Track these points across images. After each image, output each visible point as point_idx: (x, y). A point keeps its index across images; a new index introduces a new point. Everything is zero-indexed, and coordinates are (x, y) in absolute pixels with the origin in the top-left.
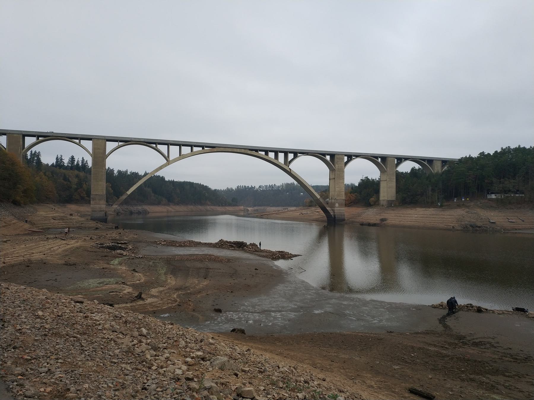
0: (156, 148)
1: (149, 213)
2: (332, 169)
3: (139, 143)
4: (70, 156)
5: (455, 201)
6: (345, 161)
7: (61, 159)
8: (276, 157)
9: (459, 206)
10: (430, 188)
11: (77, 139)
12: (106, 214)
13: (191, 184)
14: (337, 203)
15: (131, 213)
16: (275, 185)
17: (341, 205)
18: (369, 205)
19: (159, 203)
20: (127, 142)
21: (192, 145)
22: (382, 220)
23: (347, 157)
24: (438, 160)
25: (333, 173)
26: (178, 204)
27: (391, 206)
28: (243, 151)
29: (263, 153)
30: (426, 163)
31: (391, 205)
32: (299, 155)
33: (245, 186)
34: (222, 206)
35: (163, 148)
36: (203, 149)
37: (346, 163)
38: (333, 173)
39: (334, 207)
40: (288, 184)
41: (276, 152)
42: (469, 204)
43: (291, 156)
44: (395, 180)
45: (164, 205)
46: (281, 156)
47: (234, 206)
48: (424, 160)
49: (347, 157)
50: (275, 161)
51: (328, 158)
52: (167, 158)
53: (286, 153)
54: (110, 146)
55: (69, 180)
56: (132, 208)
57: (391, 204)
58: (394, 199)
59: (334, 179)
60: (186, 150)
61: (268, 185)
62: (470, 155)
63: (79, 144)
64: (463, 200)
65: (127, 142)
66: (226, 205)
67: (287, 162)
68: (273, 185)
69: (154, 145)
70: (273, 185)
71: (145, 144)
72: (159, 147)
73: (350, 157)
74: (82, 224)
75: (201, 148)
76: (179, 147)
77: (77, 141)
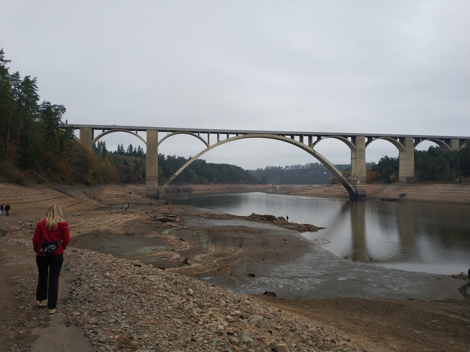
1: (193, 190)
3: (185, 132)
4: (129, 145)
7: (122, 147)
8: (301, 140)
12: (158, 192)
13: (227, 166)
14: (359, 180)
15: (179, 191)
16: (300, 165)
17: (362, 182)
19: (201, 183)
20: (175, 131)
22: (402, 195)
24: (455, 138)
26: (216, 183)
27: (410, 182)
28: (271, 136)
29: (290, 137)
30: (444, 142)
31: (410, 181)
32: (322, 137)
33: (273, 166)
34: (253, 184)
35: (204, 136)
36: (237, 135)
37: (367, 144)
40: (313, 164)
41: (301, 136)
43: (315, 139)
45: (206, 184)
46: (306, 139)
50: (300, 144)
51: (350, 139)
52: (207, 144)
53: (310, 136)
54: (161, 135)
55: (128, 164)
56: (179, 187)
58: (413, 175)
60: (223, 137)
63: (136, 135)
65: (175, 131)
66: (256, 183)
69: (197, 134)
71: (190, 133)
72: (201, 135)
73: (371, 138)
74: (139, 200)
75: (235, 135)
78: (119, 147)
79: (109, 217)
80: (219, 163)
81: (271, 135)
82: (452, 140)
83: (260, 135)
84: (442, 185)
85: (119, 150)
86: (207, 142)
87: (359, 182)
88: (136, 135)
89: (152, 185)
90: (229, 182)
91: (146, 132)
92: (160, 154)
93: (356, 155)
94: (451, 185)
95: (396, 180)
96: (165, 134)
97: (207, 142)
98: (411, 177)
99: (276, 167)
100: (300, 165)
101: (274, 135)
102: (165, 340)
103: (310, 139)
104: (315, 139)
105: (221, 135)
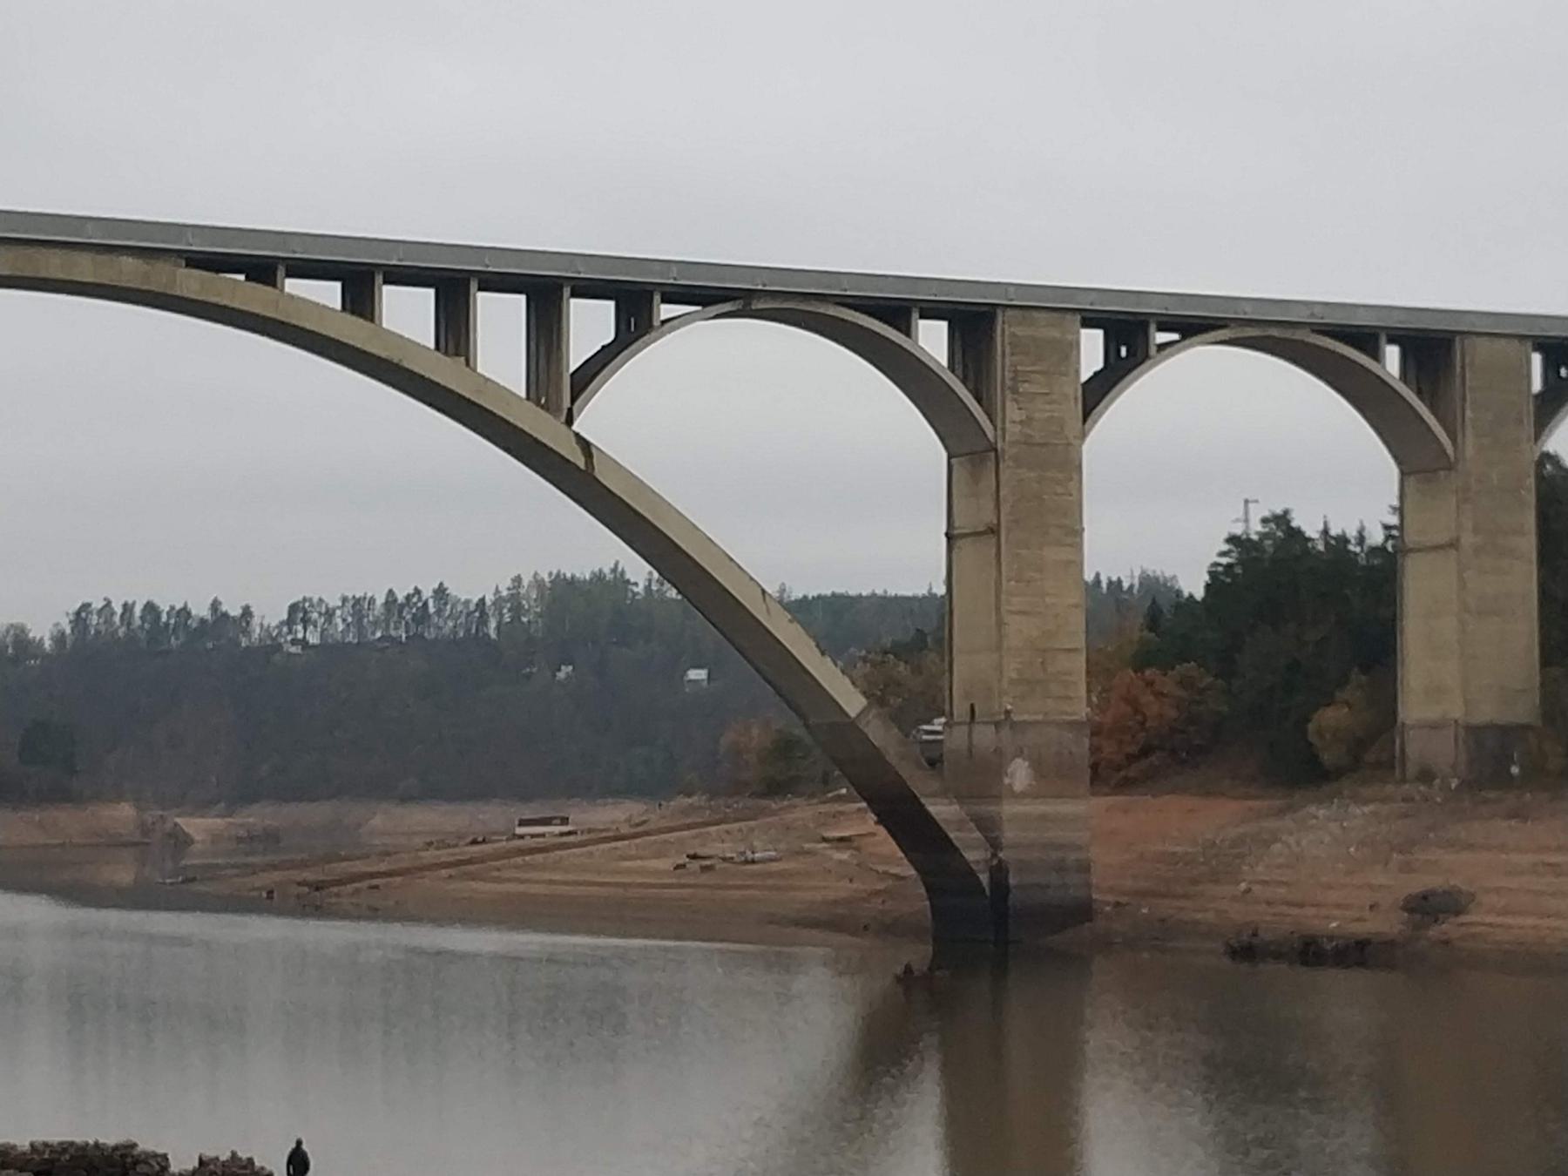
6: (1085, 375)
14: (1019, 753)
16: (440, 592)
29: (329, 293)
32: (666, 311)
33: (150, 608)
39: (997, 798)
40: (572, 583)
50: (444, 372)
51: (932, 339)
58: (1525, 710)
59: (993, 531)
61: (380, 600)
68: (427, 593)
70: (427, 593)
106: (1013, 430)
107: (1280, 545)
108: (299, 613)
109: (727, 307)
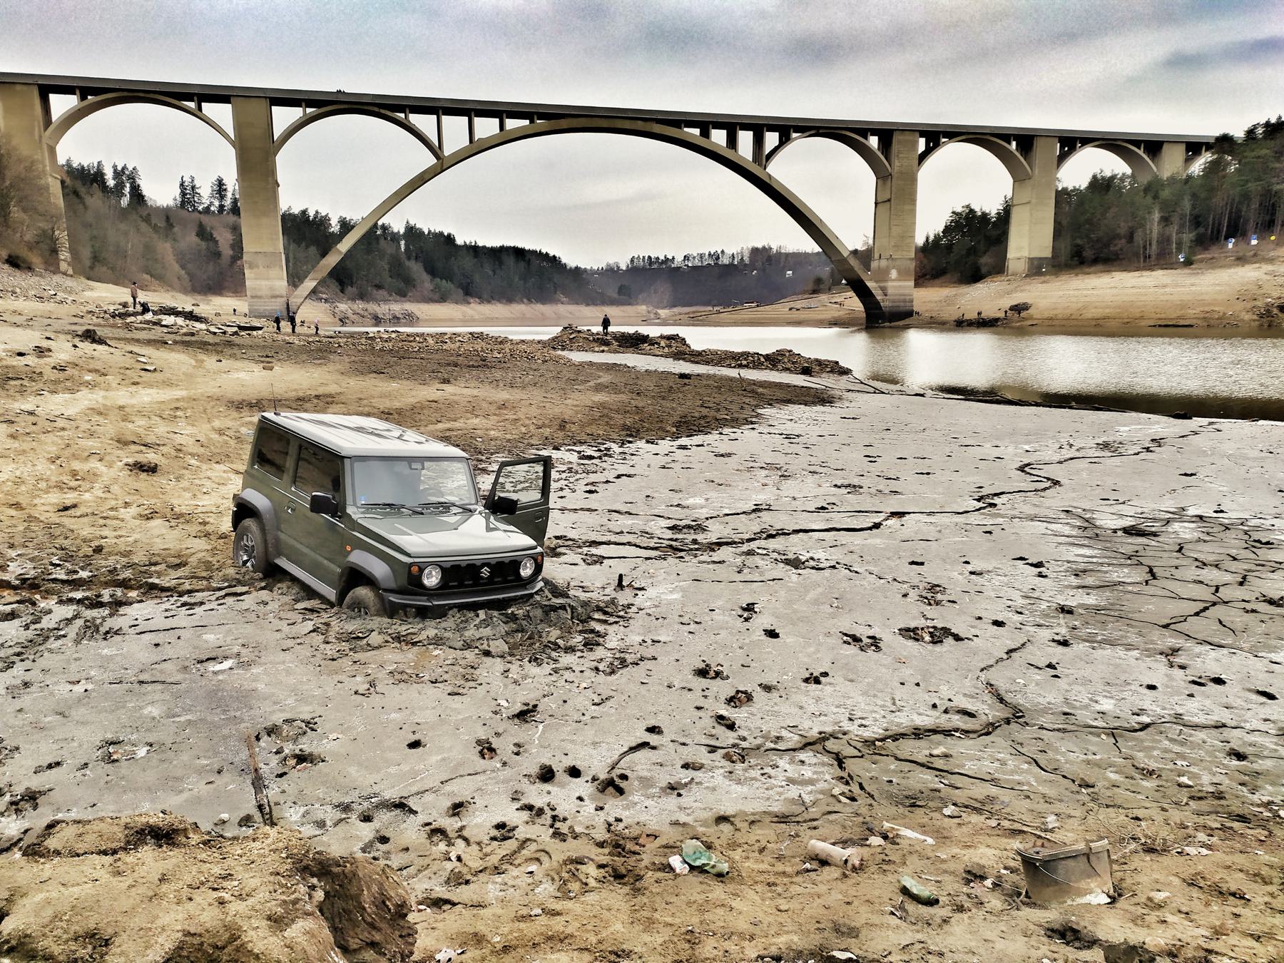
0: (405, 122)
2: (882, 176)
4: (214, 179)
5: (1230, 246)
6: (920, 152)
7: (193, 188)
8: (732, 142)
9: (1241, 260)
10: (1156, 216)
11: (189, 97)
14: (894, 267)
16: (723, 252)
17: (902, 274)
18: (975, 277)
19: (443, 299)
21: (499, 111)
22: (1019, 309)
23: (776, 135)
24: (1175, 140)
25: (884, 183)
27: (1041, 274)
28: (639, 125)
29: (696, 131)
30: (1141, 152)
31: (1037, 269)
32: (794, 135)
33: (650, 257)
35: (425, 123)
36: (532, 122)
37: (923, 157)
38: (884, 183)
39: (886, 281)
40: (757, 249)
42: (1272, 254)
43: (771, 139)
44: (1053, 201)
46: (745, 139)
47: (623, 304)
48: (1137, 141)
49: (776, 135)
50: (729, 154)
51: (873, 141)
52: (436, 151)
54: (283, 117)
55: (211, 235)
57: (1040, 267)
58: (1047, 253)
60: (487, 127)
62: (1280, 118)
63: (197, 114)
64: (1254, 242)
67: (761, 157)
71: (376, 109)
72: (416, 119)
73: (935, 136)
75: (527, 122)
76: (466, 119)
77: (192, 105)
78: (182, 185)
79: (1109, 692)
80: (494, 245)
81: (639, 122)
82: (1165, 146)
83: (605, 123)
84: (1137, 274)
85: (183, 194)
86: (437, 145)
87: (894, 274)
88: (198, 113)
89: (267, 283)
90: (525, 300)
91: (229, 106)
92: (317, 212)
93: (889, 192)
94: (1160, 272)
95: (999, 268)
96: (295, 113)
97: (434, 140)
98: (1040, 259)
99: (658, 258)
100: (723, 252)
101: (649, 123)
102: (1121, 249)
103: (759, 142)
104: (771, 139)
105: (479, 122)
106: (896, 169)
107: (968, 214)
108: (686, 258)
109: (813, 132)
